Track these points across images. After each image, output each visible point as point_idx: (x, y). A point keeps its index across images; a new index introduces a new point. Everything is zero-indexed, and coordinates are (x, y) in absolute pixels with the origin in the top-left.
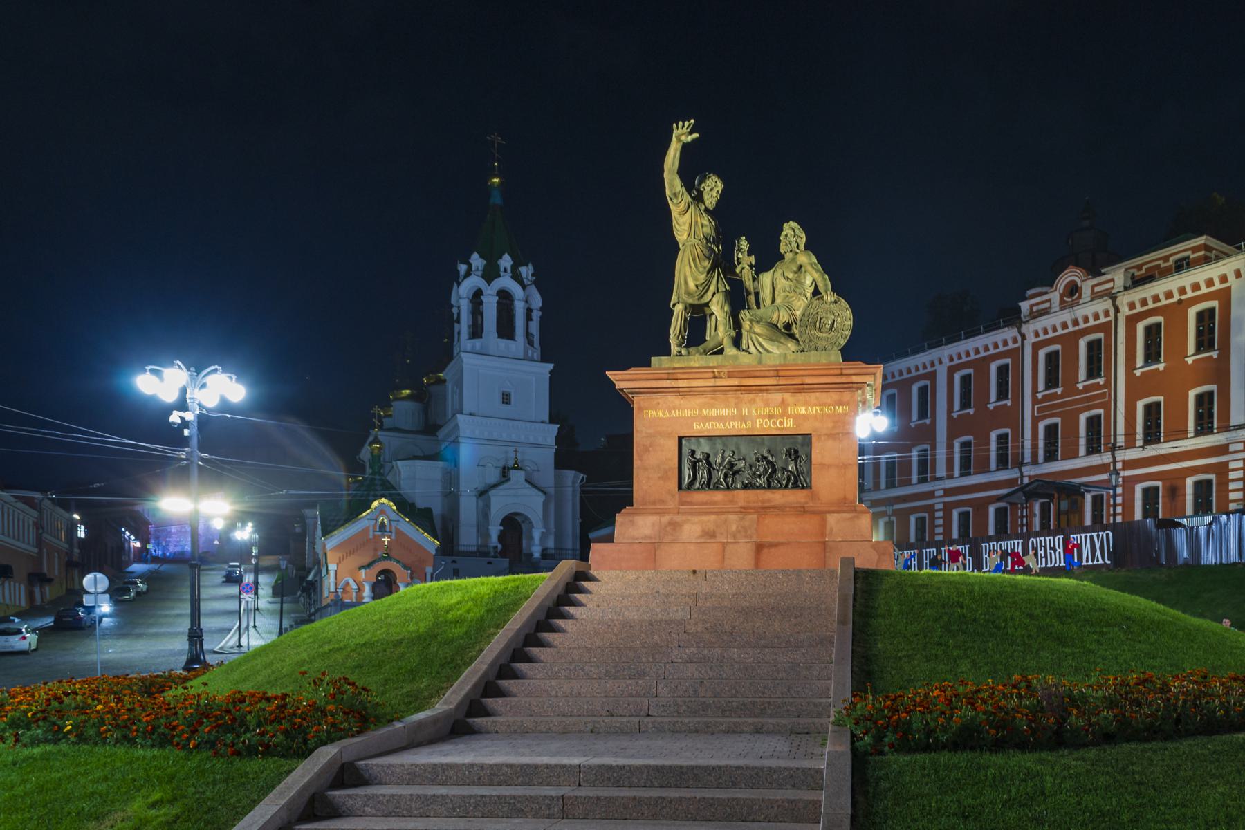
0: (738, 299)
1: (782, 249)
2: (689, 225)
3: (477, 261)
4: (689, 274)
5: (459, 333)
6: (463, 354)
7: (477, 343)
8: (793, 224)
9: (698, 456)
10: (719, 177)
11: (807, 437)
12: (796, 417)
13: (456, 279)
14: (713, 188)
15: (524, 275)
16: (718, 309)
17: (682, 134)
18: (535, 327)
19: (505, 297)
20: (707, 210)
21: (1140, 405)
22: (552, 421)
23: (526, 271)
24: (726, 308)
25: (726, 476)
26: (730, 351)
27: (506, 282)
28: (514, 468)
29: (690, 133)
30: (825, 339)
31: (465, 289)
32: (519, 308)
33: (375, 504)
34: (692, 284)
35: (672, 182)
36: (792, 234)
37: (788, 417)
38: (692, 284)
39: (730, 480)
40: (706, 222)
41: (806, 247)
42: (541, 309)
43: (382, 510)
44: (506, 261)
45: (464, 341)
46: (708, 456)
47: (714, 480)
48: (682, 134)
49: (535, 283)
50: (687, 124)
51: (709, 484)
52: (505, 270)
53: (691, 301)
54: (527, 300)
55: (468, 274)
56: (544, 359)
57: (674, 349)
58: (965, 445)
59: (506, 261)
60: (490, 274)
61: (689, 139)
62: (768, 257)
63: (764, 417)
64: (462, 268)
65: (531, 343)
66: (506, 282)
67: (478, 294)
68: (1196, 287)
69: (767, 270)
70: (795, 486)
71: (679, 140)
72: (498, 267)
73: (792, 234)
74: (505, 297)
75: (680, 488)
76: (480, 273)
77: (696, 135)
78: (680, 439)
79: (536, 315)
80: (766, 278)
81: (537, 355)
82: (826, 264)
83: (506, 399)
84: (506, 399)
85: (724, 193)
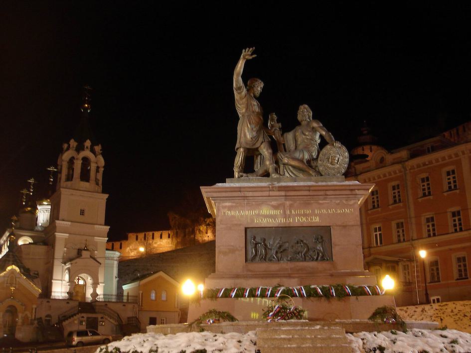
0: (275, 147)
1: (299, 118)
2: (245, 103)
3: (73, 143)
4: (246, 133)
5: (60, 179)
6: (61, 189)
7: (69, 183)
8: (306, 106)
9: (258, 240)
10: (262, 81)
11: (327, 229)
12: (320, 215)
13: (62, 151)
14: (259, 87)
15: (96, 150)
16: (265, 151)
17: (246, 54)
18: (100, 177)
19: (86, 161)
20: (255, 97)
21: (368, 218)
22: (106, 224)
23: (98, 148)
24: (270, 151)
25: (277, 252)
26: (274, 176)
27: (87, 153)
28: (84, 250)
29: (252, 55)
30: (334, 169)
31: (66, 156)
32: (93, 167)
33: (9, 268)
34: (249, 137)
35: (237, 80)
36: (305, 112)
37: (316, 215)
38: (249, 137)
39: (279, 255)
40: (255, 103)
41: (313, 118)
42: (104, 167)
43: (13, 271)
44: (88, 143)
45: (63, 183)
46: (265, 240)
47: (268, 256)
48: (246, 54)
49: (101, 154)
50: (251, 49)
51: (264, 259)
52: (87, 148)
53: (248, 147)
54: (98, 162)
55: (68, 149)
56: (104, 192)
57: (236, 175)
58: (380, 234)
59: (88, 143)
60: (80, 148)
61: (251, 58)
62: (290, 123)
63: (300, 215)
64: (65, 146)
65: (97, 184)
66: (87, 153)
67: (71, 161)
68: (444, 159)
69: (289, 131)
70: (323, 259)
71: (244, 58)
72: (84, 146)
73: (305, 112)
74: (86, 161)
75: (246, 261)
76: (74, 149)
77: (254, 56)
78: (246, 229)
79: (102, 170)
80: (290, 136)
81: (100, 189)
82: (327, 126)
83: (82, 213)
84: (82, 213)
85: (263, 89)
